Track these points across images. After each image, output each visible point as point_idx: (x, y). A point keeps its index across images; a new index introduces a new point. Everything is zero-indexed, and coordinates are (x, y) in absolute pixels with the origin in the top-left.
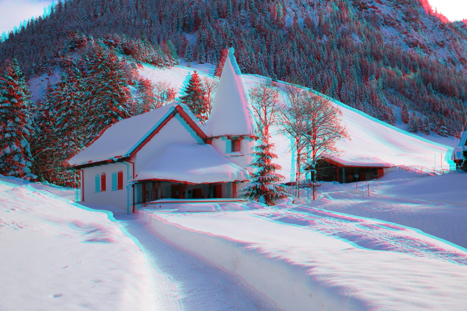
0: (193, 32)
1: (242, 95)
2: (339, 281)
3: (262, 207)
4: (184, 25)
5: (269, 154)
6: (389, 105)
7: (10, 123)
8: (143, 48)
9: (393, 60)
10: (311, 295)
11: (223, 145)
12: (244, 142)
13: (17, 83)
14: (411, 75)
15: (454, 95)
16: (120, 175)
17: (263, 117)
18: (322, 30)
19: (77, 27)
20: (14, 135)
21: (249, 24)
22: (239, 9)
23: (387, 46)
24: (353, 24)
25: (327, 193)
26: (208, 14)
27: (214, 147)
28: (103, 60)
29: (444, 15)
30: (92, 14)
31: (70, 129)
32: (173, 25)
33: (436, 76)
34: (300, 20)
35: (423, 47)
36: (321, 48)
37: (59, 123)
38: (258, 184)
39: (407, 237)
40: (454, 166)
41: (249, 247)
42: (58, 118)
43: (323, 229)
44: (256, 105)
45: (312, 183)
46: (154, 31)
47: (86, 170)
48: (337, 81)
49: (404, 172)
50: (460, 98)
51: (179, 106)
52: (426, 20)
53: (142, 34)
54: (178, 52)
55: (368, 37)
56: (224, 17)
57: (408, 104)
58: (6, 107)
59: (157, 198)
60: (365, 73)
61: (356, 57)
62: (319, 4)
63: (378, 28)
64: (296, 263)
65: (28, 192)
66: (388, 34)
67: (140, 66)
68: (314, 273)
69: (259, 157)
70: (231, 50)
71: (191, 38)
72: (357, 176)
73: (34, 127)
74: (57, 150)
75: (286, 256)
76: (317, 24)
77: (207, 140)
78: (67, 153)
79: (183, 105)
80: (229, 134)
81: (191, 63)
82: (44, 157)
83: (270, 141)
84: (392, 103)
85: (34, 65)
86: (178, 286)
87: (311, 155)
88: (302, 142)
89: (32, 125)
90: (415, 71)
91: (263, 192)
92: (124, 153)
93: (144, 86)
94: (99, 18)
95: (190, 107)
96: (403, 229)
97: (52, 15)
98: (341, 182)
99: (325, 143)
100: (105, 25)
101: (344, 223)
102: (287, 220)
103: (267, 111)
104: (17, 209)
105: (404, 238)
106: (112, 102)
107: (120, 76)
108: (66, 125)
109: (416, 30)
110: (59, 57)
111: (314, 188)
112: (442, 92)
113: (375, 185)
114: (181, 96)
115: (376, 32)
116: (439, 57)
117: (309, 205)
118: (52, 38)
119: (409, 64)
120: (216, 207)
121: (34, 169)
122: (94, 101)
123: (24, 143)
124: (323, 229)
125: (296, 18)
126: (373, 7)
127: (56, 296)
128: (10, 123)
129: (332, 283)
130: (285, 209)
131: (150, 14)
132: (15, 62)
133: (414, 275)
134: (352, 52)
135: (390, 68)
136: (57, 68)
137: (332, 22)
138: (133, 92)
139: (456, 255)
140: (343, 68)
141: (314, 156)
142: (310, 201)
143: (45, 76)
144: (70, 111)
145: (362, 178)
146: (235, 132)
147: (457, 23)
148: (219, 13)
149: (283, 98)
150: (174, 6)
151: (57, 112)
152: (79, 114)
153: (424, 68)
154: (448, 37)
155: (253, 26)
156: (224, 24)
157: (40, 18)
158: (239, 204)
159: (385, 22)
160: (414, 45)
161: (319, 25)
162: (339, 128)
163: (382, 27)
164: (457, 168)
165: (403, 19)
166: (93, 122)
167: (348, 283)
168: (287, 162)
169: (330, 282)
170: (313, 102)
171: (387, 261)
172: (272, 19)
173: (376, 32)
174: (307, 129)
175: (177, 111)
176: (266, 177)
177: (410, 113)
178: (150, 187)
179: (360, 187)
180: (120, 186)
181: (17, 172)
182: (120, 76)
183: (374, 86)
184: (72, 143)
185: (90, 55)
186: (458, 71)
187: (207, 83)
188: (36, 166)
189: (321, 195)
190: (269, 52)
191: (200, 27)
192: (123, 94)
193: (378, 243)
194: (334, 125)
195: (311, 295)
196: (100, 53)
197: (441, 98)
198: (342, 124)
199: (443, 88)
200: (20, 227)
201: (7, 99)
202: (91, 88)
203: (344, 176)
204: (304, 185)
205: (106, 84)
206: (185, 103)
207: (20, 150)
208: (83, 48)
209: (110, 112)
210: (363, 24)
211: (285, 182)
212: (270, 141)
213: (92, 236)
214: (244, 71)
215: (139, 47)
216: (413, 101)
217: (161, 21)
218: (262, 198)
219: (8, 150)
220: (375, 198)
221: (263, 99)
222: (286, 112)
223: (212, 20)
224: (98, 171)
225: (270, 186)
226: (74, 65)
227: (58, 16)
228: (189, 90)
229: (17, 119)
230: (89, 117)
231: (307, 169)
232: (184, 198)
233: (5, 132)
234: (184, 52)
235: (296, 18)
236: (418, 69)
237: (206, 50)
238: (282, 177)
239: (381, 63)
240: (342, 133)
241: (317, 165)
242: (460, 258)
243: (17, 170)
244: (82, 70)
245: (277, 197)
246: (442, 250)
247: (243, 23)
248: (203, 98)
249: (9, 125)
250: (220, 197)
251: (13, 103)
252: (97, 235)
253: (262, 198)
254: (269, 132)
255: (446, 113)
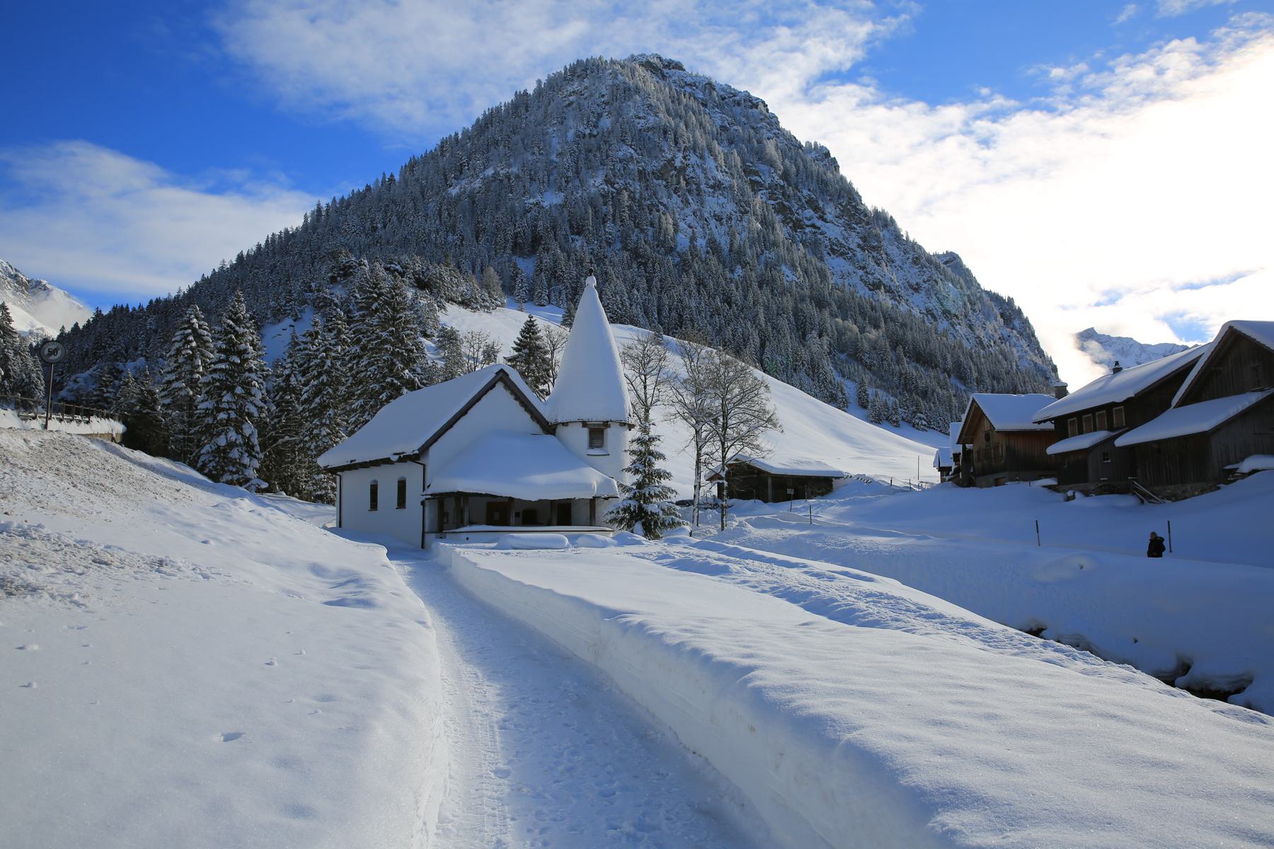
0: (529, 256)
1: (607, 354)
2: (810, 702)
3: (639, 543)
4: (516, 245)
5: (651, 454)
6: (839, 379)
7: (227, 397)
8: (447, 279)
9: (844, 309)
10: (752, 729)
11: (580, 436)
12: (609, 433)
13: (240, 330)
14: (873, 334)
15: (936, 366)
16: (402, 485)
17: (642, 393)
18: (737, 257)
19: (345, 245)
20: (233, 415)
21: (619, 246)
22: (604, 222)
23: (835, 287)
24: (782, 251)
25: (743, 519)
26: (554, 228)
27: (560, 440)
28: (380, 295)
29: (920, 243)
30: (368, 225)
31: (324, 407)
32: (496, 243)
33: (909, 336)
34: (701, 243)
35: (889, 290)
36: (733, 286)
37: (305, 396)
38: (633, 503)
39: (881, 594)
40: (935, 476)
41: (624, 620)
42: (305, 389)
43: (744, 582)
44: (630, 373)
45: (720, 502)
46: (467, 252)
47: (347, 476)
48: (757, 340)
49: (866, 484)
50: (945, 370)
51: (502, 370)
52: (894, 251)
53: (446, 256)
54: (503, 287)
55: (806, 272)
56: (579, 234)
57: (867, 377)
58: (221, 370)
59: (461, 524)
60: (802, 329)
61: (788, 302)
62: (730, 219)
63: (821, 259)
64: (719, 659)
65: (245, 507)
66: (838, 269)
67: (442, 307)
68: (758, 683)
69: (635, 457)
70: (592, 281)
71: (526, 266)
72: (790, 491)
73: (265, 402)
74: (301, 441)
75: (698, 643)
76: (726, 248)
77: (549, 429)
78: (316, 447)
79: (509, 370)
80: (585, 418)
81: (524, 305)
82: (280, 453)
83: (653, 432)
84: (844, 376)
85: (272, 303)
86: (492, 691)
87: (719, 455)
88: (704, 435)
89: (263, 400)
90: (877, 327)
91: (643, 516)
92: (412, 448)
93: (449, 338)
94: (380, 232)
95: (522, 374)
96: (871, 580)
97: (305, 226)
98: (766, 501)
99: (741, 438)
100: (388, 243)
101: (778, 570)
102: (685, 565)
103: (648, 382)
104: (212, 542)
105: (875, 595)
106: (393, 364)
107: (407, 322)
108: (317, 400)
109: (879, 265)
110: (311, 291)
111: (723, 510)
112: (918, 361)
113: (818, 506)
114: (508, 356)
115: (819, 264)
116: (913, 307)
117: (715, 538)
118: (304, 262)
119: (871, 316)
120: (563, 541)
121: (264, 473)
122: (364, 362)
123: (249, 428)
124: (744, 582)
125: (693, 239)
126: (813, 226)
127: (229, 738)
128: (227, 397)
129: (799, 708)
130: (681, 545)
131: (460, 226)
132: (238, 297)
133: (949, 686)
134: (783, 294)
135: (839, 320)
136: (308, 309)
137: (751, 247)
138: (429, 348)
139: (966, 625)
140: (768, 320)
141: (724, 457)
142: (715, 532)
143: (289, 321)
144: (324, 378)
145: (799, 495)
146: (597, 416)
147: (938, 256)
148: (571, 227)
149: (676, 364)
150: (499, 215)
151: (303, 380)
152: (340, 383)
153: (891, 324)
154: (925, 278)
155: (625, 248)
156: (578, 244)
157: (287, 231)
158: (599, 536)
159: (832, 250)
160: (876, 286)
161: (731, 250)
162: (765, 412)
163: (826, 257)
164: (943, 480)
165: (859, 246)
166: (360, 396)
167: (833, 709)
168: (682, 468)
169: (793, 705)
170: (722, 370)
171: (890, 654)
172: (656, 238)
173: (819, 264)
174: (713, 415)
175: (502, 376)
176: (646, 491)
177: (870, 391)
178: (450, 506)
179: (796, 510)
180: (401, 503)
181: (236, 477)
182: (407, 322)
183: (815, 348)
184: (325, 431)
185: (361, 289)
186: (940, 329)
187: (549, 336)
188: (267, 467)
189: (734, 522)
190: (650, 290)
191: (541, 248)
192: (412, 351)
193: (839, 606)
194: (757, 407)
195: (752, 729)
196: (376, 285)
197: (917, 370)
198: (769, 407)
199: (919, 354)
200: (205, 577)
201: (223, 356)
202: (359, 341)
203: (770, 491)
204: (706, 506)
205: (384, 334)
206: (514, 367)
207: (240, 441)
208: (351, 278)
209: (389, 380)
210: (800, 251)
211: (679, 498)
212: (653, 432)
213: (339, 593)
214: (612, 320)
215: (441, 278)
216: (874, 374)
217: (477, 238)
218: (638, 526)
219: (222, 441)
220: (821, 526)
221: (642, 364)
222: (678, 385)
223: (560, 237)
224: (366, 477)
225: (652, 508)
226: (336, 305)
227: (315, 229)
228: (520, 346)
229: (239, 390)
230: (355, 388)
231: (711, 479)
232: (507, 524)
233: (219, 410)
234: (514, 288)
235: (693, 239)
236: (883, 324)
237: (550, 286)
238: (673, 491)
239: (826, 313)
240: (769, 420)
241: (728, 473)
242: (974, 631)
243: (236, 473)
244: (348, 312)
245: (663, 524)
246: (941, 616)
247: (609, 244)
248: (544, 360)
249: (225, 399)
250: (569, 524)
251: (233, 363)
252: (352, 592)
253: (638, 526)
254: (651, 417)
255: (924, 394)
